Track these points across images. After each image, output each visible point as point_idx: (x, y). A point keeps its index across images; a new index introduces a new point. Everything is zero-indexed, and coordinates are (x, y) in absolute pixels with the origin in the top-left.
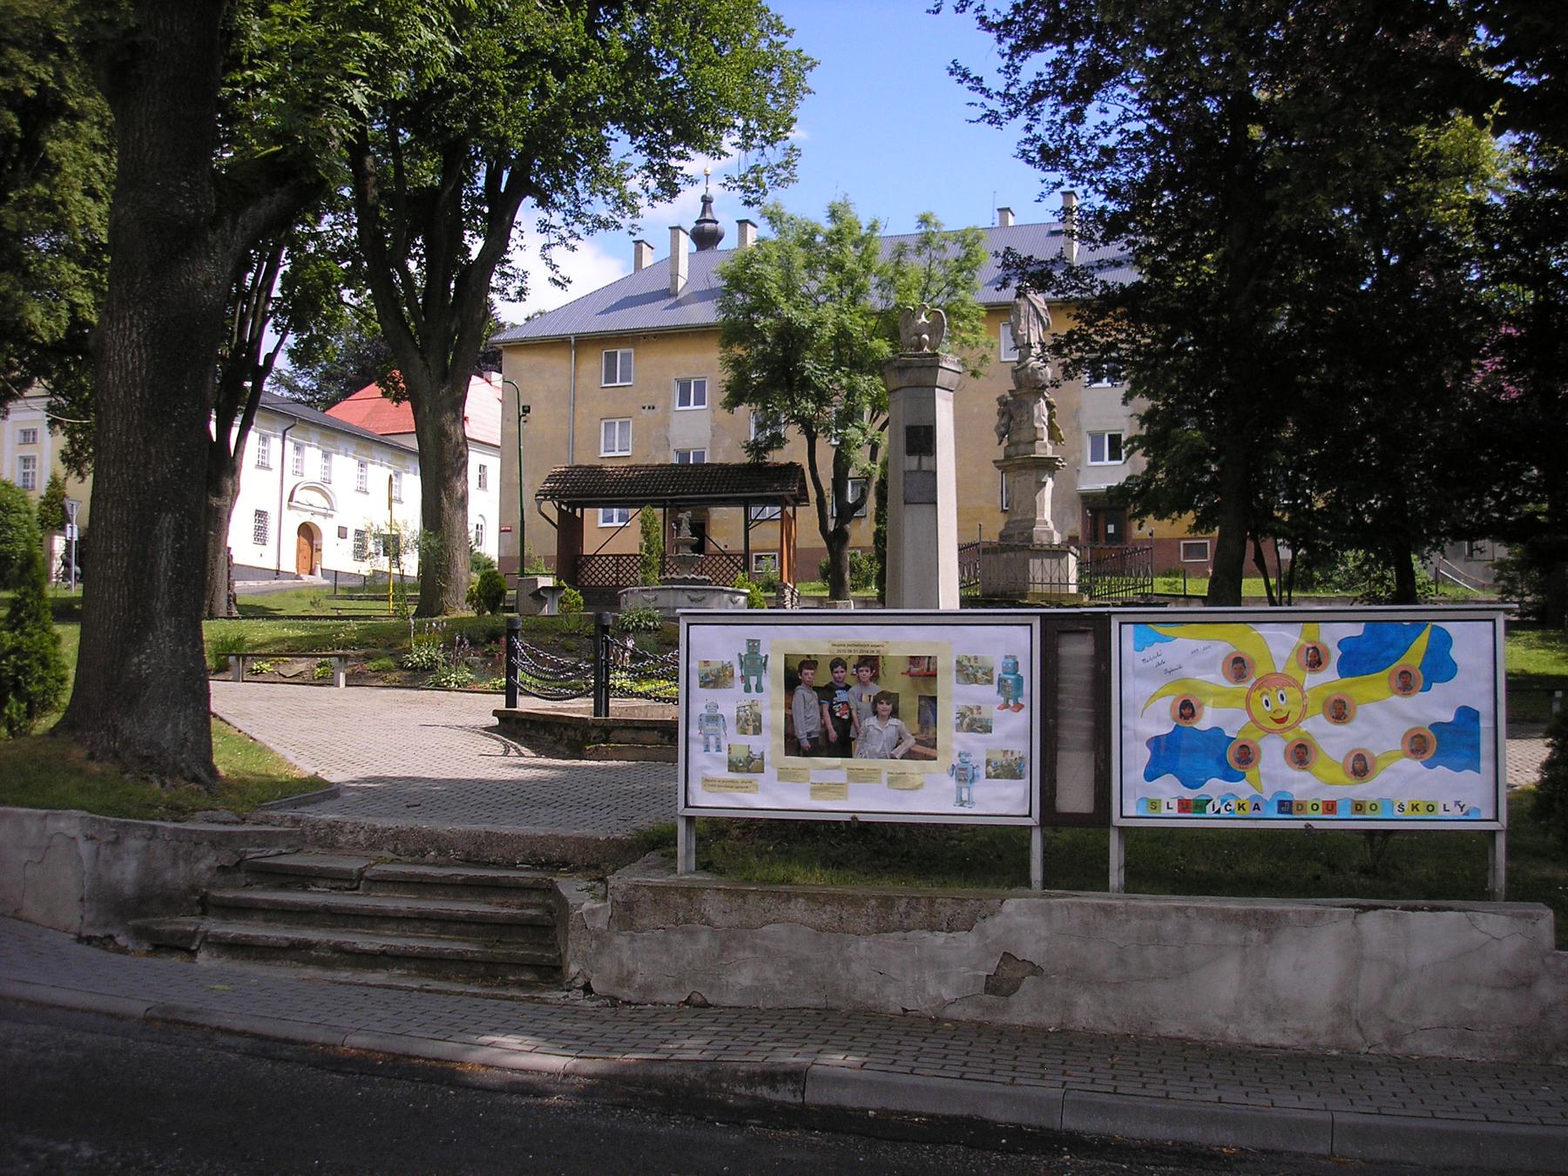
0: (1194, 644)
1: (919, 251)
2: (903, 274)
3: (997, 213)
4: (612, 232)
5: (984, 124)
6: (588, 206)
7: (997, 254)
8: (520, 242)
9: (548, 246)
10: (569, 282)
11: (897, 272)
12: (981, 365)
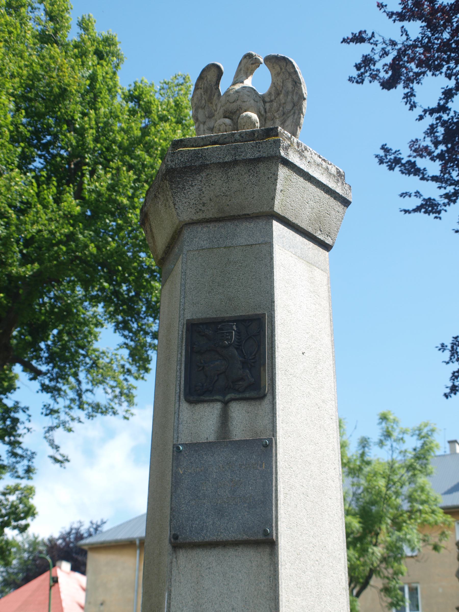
0: (282, 540)
1: (381, 443)
2: (368, 463)
3: (448, 445)
4: (109, 418)
5: (421, 215)
6: (89, 394)
7: (443, 347)
8: (28, 425)
9: (51, 429)
10: (68, 460)
11: (363, 461)
12: (440, 540)
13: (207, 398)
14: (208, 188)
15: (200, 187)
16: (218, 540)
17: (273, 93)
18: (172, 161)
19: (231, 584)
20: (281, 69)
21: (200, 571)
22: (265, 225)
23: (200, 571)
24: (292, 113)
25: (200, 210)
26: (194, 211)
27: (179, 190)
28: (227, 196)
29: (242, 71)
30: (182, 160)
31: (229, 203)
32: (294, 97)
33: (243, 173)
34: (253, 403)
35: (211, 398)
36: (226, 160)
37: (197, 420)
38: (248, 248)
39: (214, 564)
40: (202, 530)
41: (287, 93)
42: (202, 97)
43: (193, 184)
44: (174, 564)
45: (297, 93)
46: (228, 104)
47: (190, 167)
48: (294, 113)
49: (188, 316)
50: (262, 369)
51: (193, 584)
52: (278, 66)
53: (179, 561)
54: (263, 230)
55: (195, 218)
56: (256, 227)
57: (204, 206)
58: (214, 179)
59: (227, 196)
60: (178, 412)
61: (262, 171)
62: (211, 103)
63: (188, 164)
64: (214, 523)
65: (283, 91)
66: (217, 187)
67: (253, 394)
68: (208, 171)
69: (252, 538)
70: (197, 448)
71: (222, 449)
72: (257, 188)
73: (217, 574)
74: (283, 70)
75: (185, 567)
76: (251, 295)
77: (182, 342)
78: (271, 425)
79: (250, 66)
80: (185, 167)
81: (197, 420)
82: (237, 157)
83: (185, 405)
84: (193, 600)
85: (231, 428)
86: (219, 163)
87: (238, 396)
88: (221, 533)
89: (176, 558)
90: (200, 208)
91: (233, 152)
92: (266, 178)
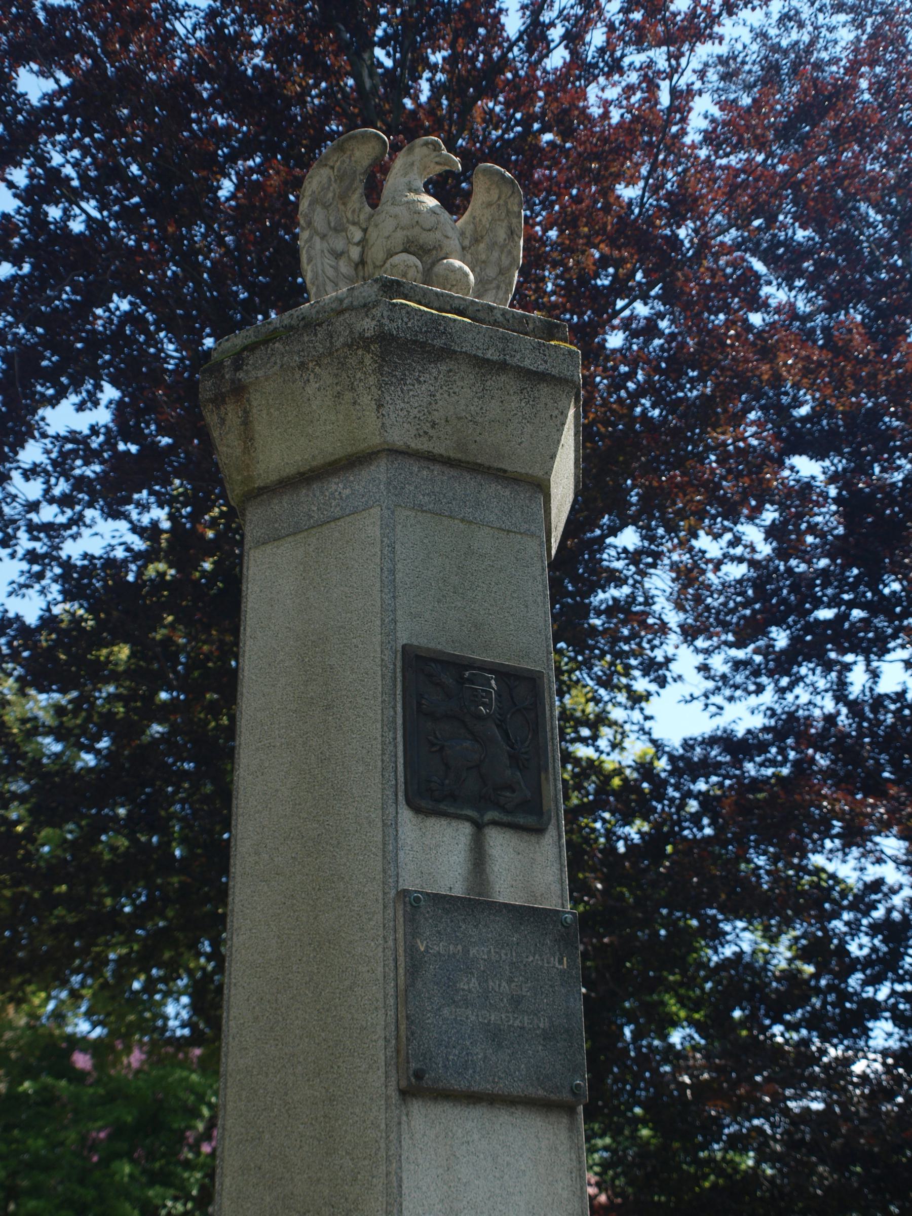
13: (452, 810)
14: (446, 396)
15: (432, 389)
16: (495, 1092)
17: (468, 235)
18: (392, 320)
19: (506, 1177)
20: (499, 198)
21: (451, 1146)
22: (530, 500)
23: (451, 1146)
24: (494, 285)
25: (426, 433)
26: (413, 432)
27: (394, 380)
28: (476, 423)
29: (415, 168)
30: (410, 325)
31: (478, 439)
32: (503, 258)
33: (511, 392)
34: (525, 836)
35: (459, 812)
36: (488, 356)
37: (431, 849)
38: (503, 535)
39: (476, 1137)
40: (466, 1069)
41: (492, 246)
42: (330, 185)
43: (422, 379)
44: (404, 1126)
45: (510, 252)
46: (417, 229)
47: (423, 345)
48: (498, 287)
49: (403, 638)
50: (543, 776)
51: (440, 1171)
52: (497, 191)
53: (413, 1123)
54: (526, 509)
55: (413, 445)
56: (515, 499)
57: (433, 427)
58: (459, 383)
59: (476, 423)
60: (391, 826)
61: (543, 399)
62: (344, 204)
63: (421, 338)
64: (485, 1057)
65: (487, 239)
66: (463, 402)
67: (531, 821)
68: (452, 365)
69: (553, 1097)
70: (447, 906)
71: (492, 917)
72: (529, 429)
73: (482, 1156)
74: (501, 202)
75: (424, 1135)
76: (512, 627)
77: (395, 686)
78: (559, 886)
79: (432, 165)
80: (415, 342)
81: (431, 849)
82: (507, 357)
83: (406, 815)
84: (442, 1201)
85: (492, 878)
86: (475, 356)
87: (506, 819)
88: (500, 1078)
89: (407, 1115)
90: (425, 428)
91: (501, 346)
92: (547, 415)
